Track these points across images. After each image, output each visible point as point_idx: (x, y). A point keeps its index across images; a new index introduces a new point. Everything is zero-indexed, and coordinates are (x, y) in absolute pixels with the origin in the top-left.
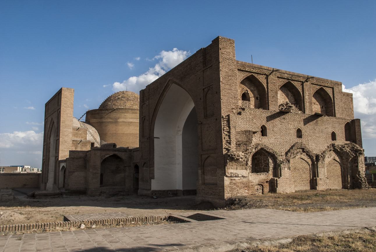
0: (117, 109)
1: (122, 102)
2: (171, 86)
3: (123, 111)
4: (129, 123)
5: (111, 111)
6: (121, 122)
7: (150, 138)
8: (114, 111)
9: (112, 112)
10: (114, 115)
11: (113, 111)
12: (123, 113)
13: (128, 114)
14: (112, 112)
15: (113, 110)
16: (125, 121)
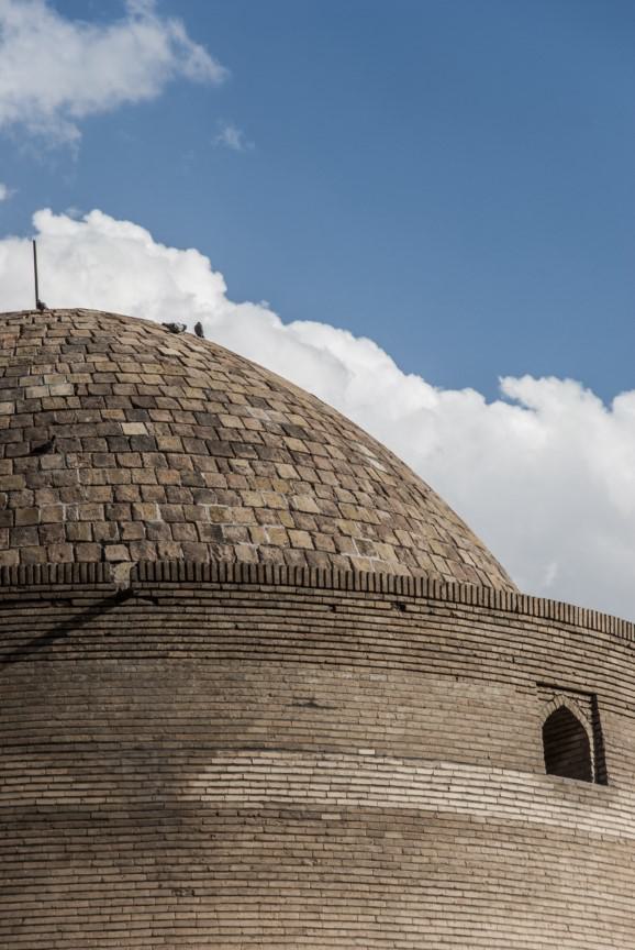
0: (155, 583)
1: (139, 473)
2: (229, 946)
3: (268, 622)
4: (376, 836)
5: (43, 616)
6: (243, 815)
7: (196, 437)
8: (105, 621)
9: (61, 631)
10: (105, 689)
11: (77, 622)
12: (259, 649)
13: (346, 674)
14: (61, 631)
15: (85, 599)
16: (321, 795)
